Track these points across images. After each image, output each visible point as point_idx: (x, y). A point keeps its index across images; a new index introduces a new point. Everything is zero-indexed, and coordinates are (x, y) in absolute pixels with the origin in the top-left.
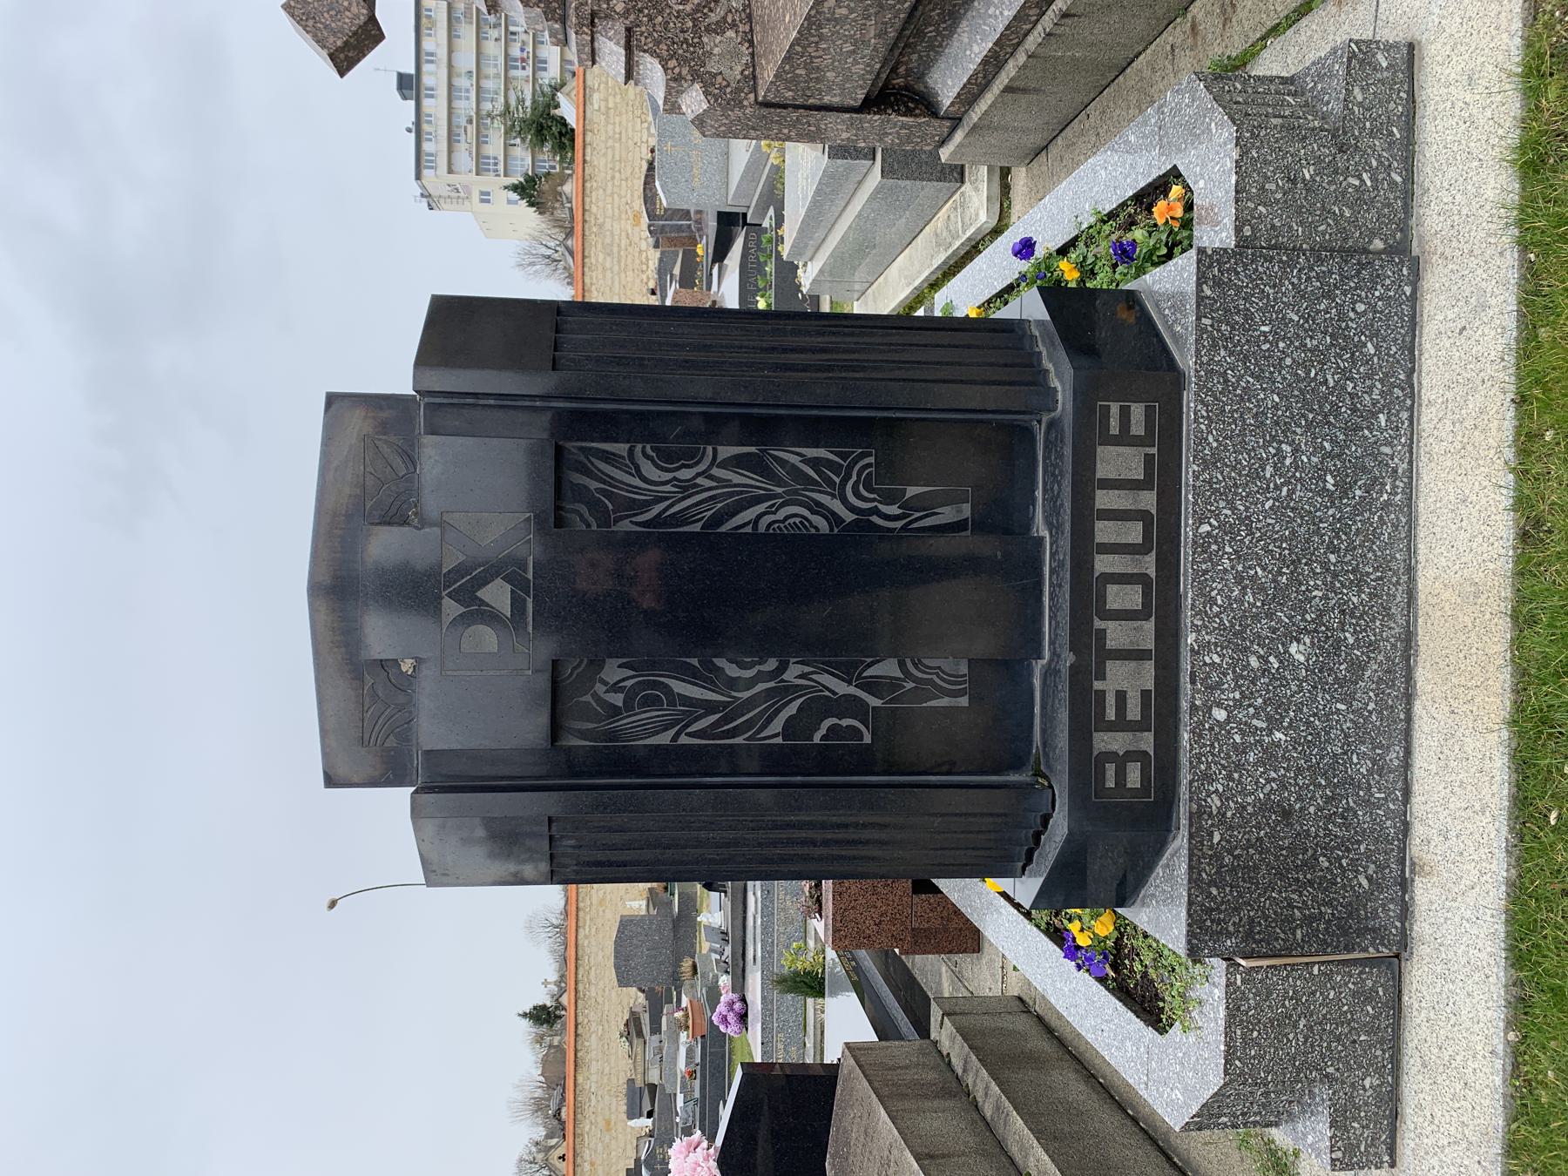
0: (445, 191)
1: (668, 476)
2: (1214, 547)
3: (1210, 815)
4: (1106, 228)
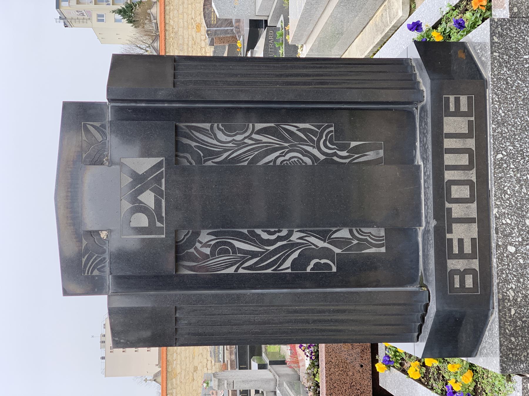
0: (75, 15)
1: (230, 139)
2: (505, 165)
3: (509, 300)
4: (455, 13)
